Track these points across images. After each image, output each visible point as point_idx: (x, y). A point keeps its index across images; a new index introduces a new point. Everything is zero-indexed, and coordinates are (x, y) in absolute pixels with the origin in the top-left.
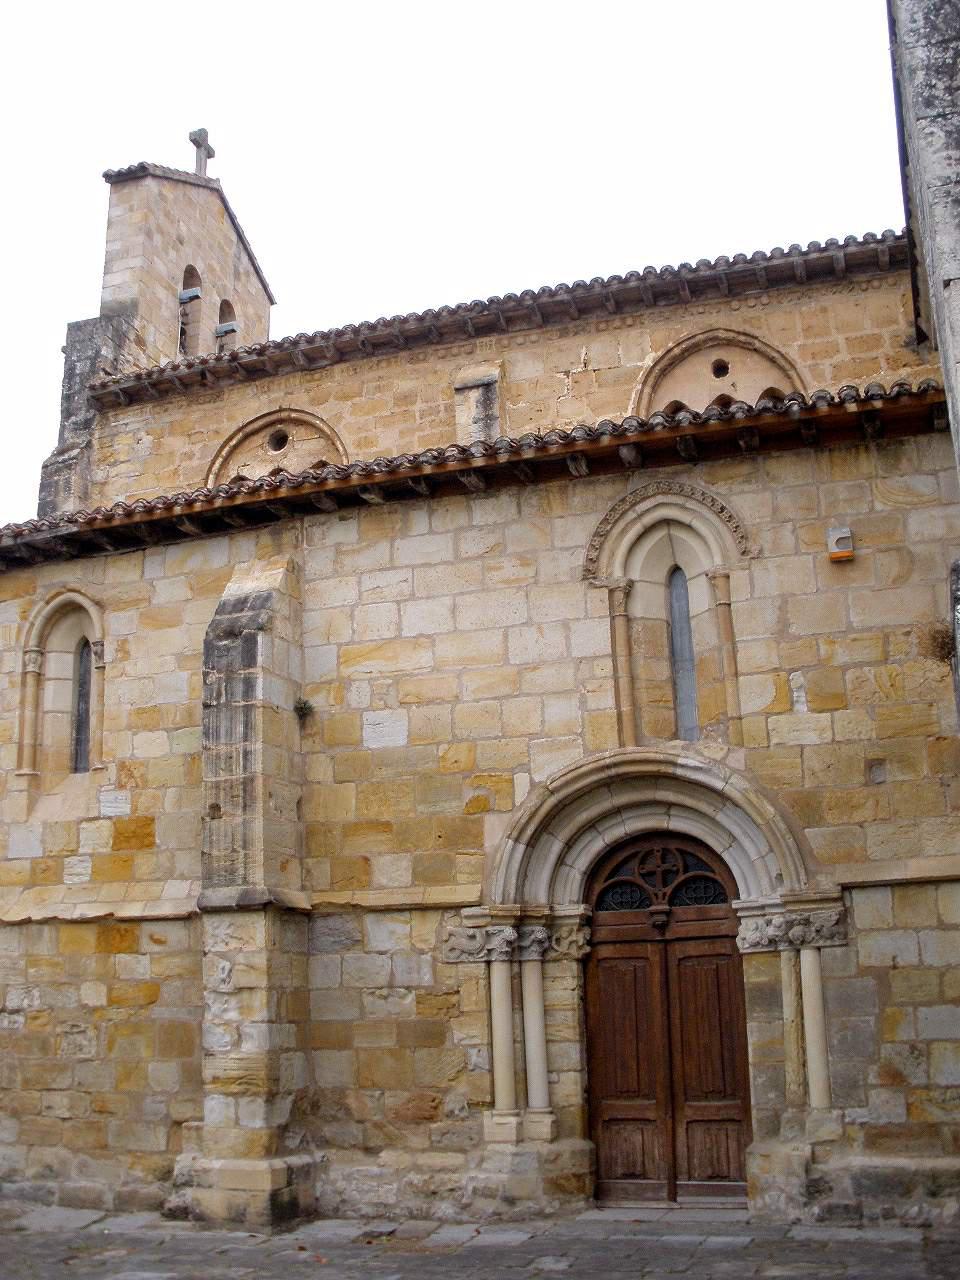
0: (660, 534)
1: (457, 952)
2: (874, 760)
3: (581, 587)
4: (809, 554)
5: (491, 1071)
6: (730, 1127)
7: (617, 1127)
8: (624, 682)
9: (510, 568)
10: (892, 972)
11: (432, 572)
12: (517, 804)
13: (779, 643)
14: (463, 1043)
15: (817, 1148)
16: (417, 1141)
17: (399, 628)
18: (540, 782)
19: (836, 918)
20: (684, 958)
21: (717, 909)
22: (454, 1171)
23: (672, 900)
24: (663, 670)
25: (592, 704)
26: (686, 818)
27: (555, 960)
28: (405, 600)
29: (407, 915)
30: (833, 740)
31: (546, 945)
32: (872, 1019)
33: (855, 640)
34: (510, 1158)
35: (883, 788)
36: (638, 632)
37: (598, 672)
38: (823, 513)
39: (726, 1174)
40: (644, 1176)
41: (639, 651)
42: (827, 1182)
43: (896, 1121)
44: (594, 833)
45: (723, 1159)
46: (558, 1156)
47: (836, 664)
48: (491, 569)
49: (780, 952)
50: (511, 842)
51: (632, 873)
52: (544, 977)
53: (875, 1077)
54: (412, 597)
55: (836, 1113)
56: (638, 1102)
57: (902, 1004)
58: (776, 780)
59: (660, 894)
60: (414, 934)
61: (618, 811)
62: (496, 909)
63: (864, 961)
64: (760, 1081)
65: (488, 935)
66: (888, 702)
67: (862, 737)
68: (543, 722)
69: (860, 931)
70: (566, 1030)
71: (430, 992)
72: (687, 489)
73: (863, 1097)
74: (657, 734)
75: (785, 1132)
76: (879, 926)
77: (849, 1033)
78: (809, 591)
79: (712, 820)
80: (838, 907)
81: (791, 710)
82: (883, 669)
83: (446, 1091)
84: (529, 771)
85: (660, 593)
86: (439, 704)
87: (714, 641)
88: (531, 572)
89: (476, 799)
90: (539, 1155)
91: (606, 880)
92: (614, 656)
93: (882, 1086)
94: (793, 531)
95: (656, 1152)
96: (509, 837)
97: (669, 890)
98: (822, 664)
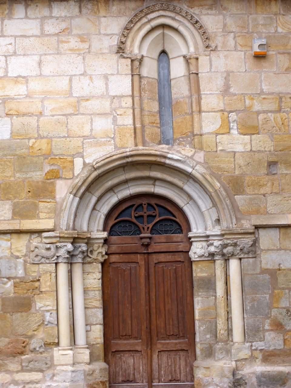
0: (158, 32)
1: (39, 258)
2: (272, 162)
3: (115, 57)
4: (242, 51)
5: (58, 325)
6: (182, 353)
7: (119, 355)
8: (137, 111)
9: (74, 43)
10: (278, 272)
11: (27, 40)
12: (76, 175)
13: (224, 97)
14: (42, 309)
15: (238, 363)
16: (13, 366)
17: (6, 71)
18: (89, 164)
19: (252, 243)
20: (158, 263)
21: (178, 237)
22: (37, 383)
23: (153, 231)
24: (155, 107)
25: (120, 121)
26: (168, 188)
27: (90, 263)
28: (10, 56)
29: (8, 236)
30: (251, 150)
31: (85, 254)
32: (268, 296)
33: (264, 98)
34: (70, 374)
35: (276, 176)
36: (144, 84)
37: (123, 104)
38: (251, 30)
39: (179, 379)
40: (134, 381)
41: (145, 95)
42: (244, 380)
43: (278, 348)
44: (113, 193)
45: (178, 371)
46: (94, 371)
47: (254, 110)
48: (63, 42)
49: (214, 261)
50: (72, 196)
51: (132, 216)
52: (84, 272)
53: (268, 326)
54: (15, 54)
55: (248, 344)
56: (132, 341)
57: (283, 289)
58: (219, 169)
59: (146, 228)
60: (13, 247)
61: (126, 182)
62: (63, 233)
63: (264, 266)
64: (202, 328)
65: (57, 248)
66: (281, 133)
67: (266, 149)
68: (92, 130)
69: (262, 250)
70: (95, 302)
71: (22, 280)
72: (178, 9)
73: (262, 336)
74: (153, 140)
75: (218, 355)
76: (272, 248)
77: (256, 303)
78: (241, 71)
79: (181, 189)
80: (252, 237)
81: (229, 132)
82: (278, 115)
83: (31, 337)
84: (83, 157)
85: (155, 64)
86: (30, 116)
87: (186, 93)
88: (86, 45)
89: (51, 171)
90: (84, 371)
91: (115, 220)
92: (133, 96)
93: (272, 330)
94: (235, 38)
95: (141, 368)
96: (71, 193)
97: (150, 226)
98: (247, 110)
